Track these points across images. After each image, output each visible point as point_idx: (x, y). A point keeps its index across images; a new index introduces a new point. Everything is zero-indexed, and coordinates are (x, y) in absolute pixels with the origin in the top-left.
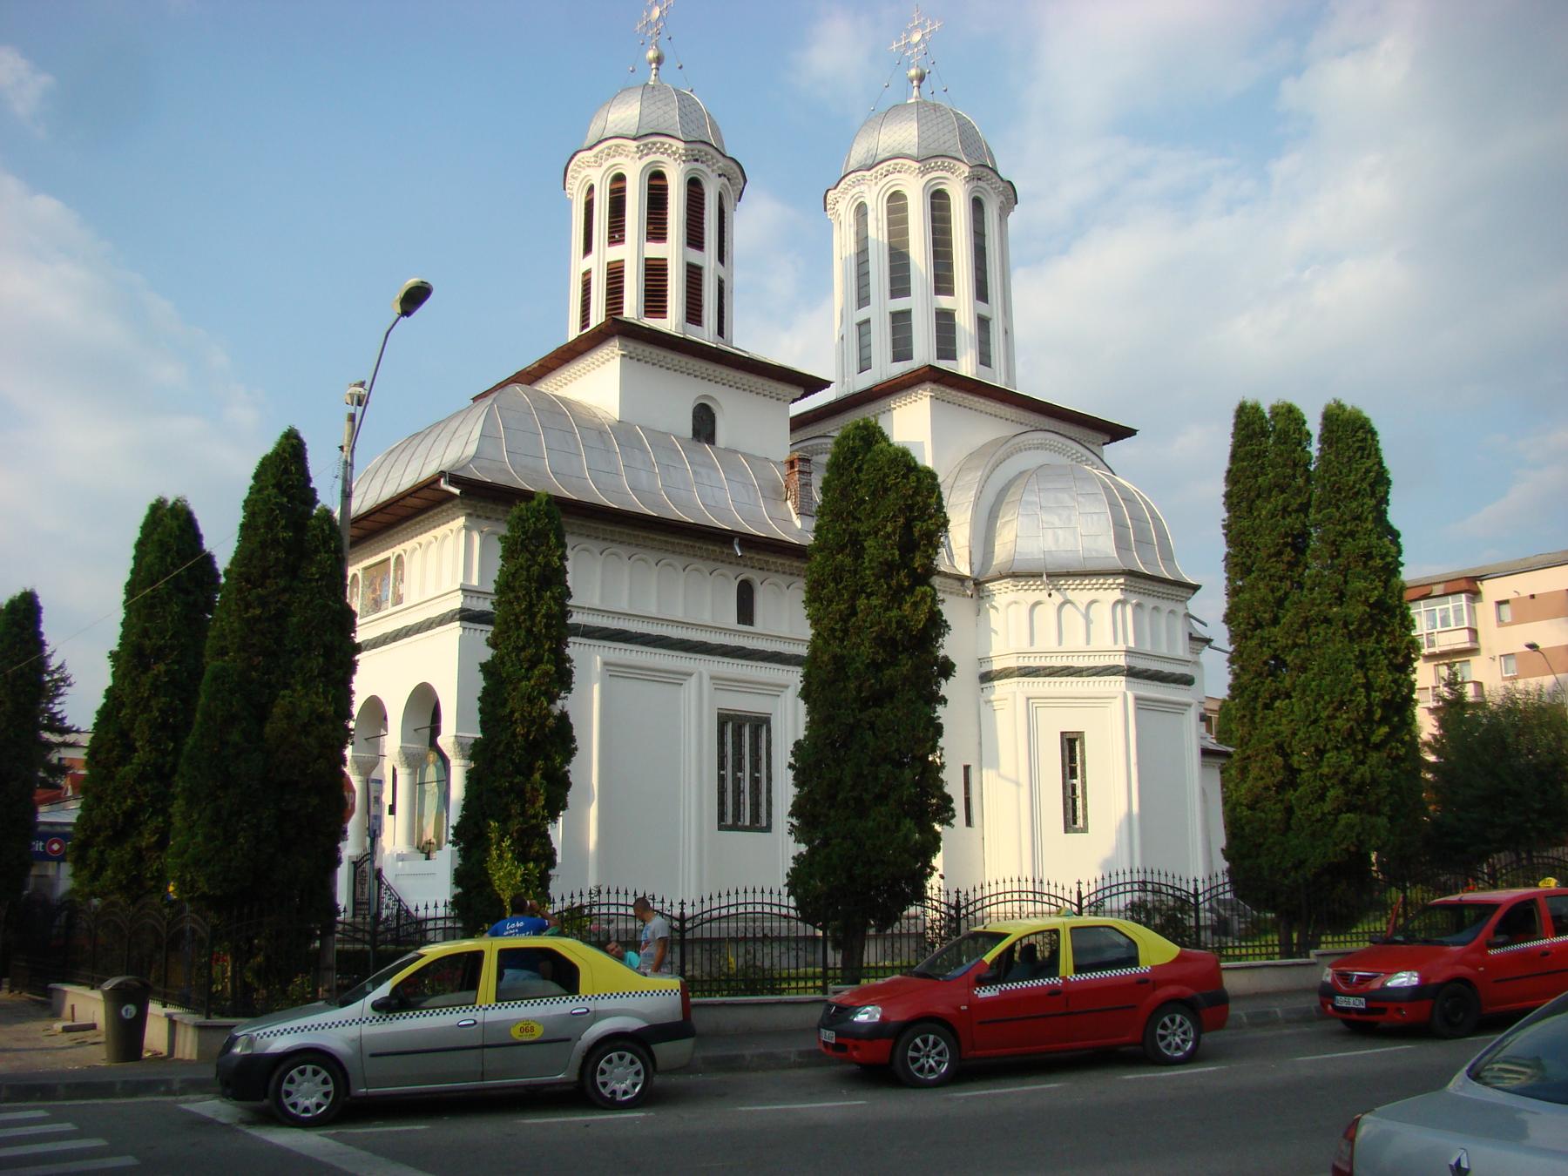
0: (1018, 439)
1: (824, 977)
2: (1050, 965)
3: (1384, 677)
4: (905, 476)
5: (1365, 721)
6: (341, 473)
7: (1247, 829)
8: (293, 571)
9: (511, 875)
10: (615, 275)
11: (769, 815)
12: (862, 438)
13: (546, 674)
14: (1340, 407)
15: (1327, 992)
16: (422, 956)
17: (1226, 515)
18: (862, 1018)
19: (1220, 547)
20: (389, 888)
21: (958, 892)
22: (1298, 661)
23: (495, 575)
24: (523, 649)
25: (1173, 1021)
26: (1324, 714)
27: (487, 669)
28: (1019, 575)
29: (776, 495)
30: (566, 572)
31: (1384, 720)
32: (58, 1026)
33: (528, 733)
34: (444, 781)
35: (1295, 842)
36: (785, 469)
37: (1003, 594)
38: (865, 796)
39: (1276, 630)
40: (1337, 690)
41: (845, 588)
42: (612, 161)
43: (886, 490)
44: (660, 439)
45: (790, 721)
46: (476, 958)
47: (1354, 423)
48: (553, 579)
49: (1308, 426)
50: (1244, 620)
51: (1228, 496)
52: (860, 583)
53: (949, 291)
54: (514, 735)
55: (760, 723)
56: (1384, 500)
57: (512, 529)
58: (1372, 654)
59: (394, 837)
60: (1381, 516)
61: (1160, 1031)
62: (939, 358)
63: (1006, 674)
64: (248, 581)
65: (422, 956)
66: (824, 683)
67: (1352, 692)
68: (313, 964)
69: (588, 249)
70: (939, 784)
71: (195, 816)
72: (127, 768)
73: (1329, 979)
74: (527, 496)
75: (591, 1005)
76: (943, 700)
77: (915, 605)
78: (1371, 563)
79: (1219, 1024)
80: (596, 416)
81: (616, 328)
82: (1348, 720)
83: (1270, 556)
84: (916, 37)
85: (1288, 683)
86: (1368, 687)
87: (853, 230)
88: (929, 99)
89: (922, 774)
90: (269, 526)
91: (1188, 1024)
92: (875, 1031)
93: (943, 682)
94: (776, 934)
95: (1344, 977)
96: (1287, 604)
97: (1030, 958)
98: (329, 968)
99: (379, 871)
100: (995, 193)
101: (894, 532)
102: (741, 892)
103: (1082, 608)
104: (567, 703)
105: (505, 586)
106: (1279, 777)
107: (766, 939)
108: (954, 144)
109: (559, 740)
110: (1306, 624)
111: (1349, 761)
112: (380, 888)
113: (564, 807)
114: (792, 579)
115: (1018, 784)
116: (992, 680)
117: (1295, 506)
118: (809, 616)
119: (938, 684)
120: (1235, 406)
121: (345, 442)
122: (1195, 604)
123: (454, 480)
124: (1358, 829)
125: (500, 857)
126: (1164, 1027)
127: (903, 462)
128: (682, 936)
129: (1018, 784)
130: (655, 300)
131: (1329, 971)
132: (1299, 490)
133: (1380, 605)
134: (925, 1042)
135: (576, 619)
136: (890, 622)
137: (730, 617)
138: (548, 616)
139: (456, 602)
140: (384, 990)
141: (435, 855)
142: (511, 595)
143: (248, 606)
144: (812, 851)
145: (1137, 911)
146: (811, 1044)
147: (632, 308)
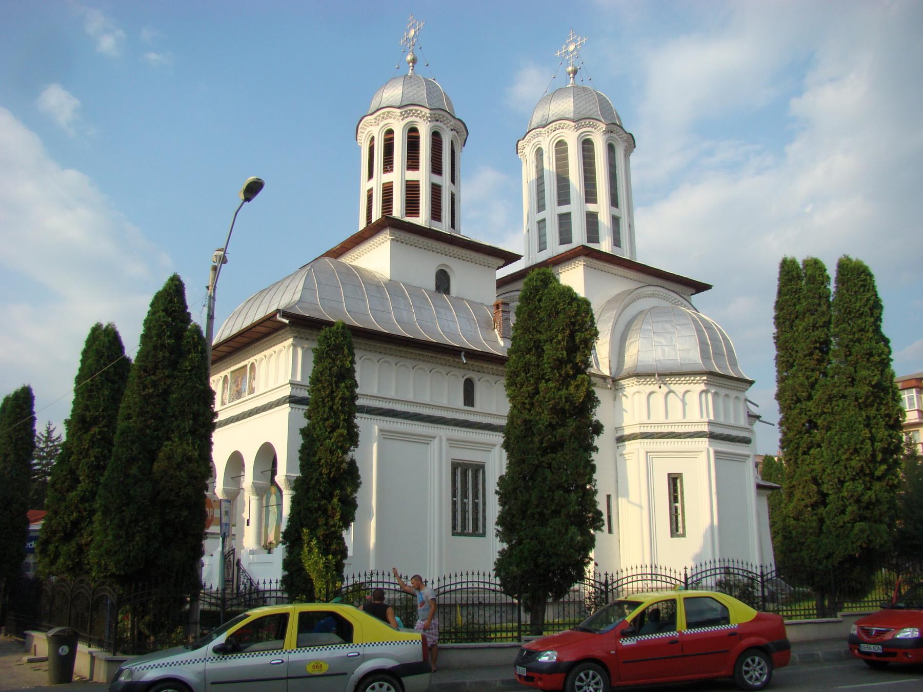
0: (636, 292)
1: (519, 629)
2: (670, 622)
3: (882, 433)
4: (570, 304)
5: (871, 461)
6: (207, 304)
7: (794, 532)
8: (174, 365)
9: (316, 563)
10: (388, 191)
11: (484, 526)
12: (541, 281)
13: (342, 435)
14: (849, 259)
15: (854, 642)
16: (248, 616)
17: (775, 331)
18: (544, 659)
19: (772, 351)
20: (244, 571)
21: (606, 574)
22: (825, 423)
23: (310, 373)
24: (327, 419)
25: (753, 661)
26: (843, 457)
27: (305, 432)
28: (640, 375)
29: (488, 326)
30: (354, 371)
31: (883, 461)
32: (25, 658)
33: (330, 473)
34: (280, 505)
35: (825, 541)
36: (494, 310)
37: (631, 387)
38: (546, 512)
39: (810, 403)
40: (852, 441)
41: (531, 376)
42: (385, 122)
43: (557, 313)
44: (415, 291)
45: (497, 464)
46: (283, 618)
47: (859, 269)
48: (346, 375)
49: (828, 273)
50: (789, 398)
51: (777, 318)
52: (541, 373)
53: (595, 201)
54: (321, 474)
55: (479, 468)
56: (879, 319)
57: (320, 345)
58: (874, 418)
59: (249, 539)
60: (877, 330)
61: (744, 668)
62: (588, 242)
63: (633, 437)
64: (145, 371)
65: (248, 616)
66: (518, 437)
67: (862, 443)
68: (185, 620)
69: (371, 175)
70: (594, 503)
71: (108, 523)
72: (74, 493)
73: (855, 632)
74: (330, 324)
75: (360, 650)
76: (596, 449)
77: (577, 387)
78: (871, 359)
79: (785, 663)
80: (375, 276)
81: (388, 222)
82: (860, 461)
83: (805, 356)
84: (572, 48)
85: (818, 437)
86: (873, 439)
87: (534, 165)
88: (581, 84)
89: (583, 497)
90: (159, 336)
91: (763, 663)
92: (553, 668)
93: (596, 437)
94: (487, 602)
95: (867, 632)
96: (817, 386)
97: (658, 617)
98: (196, 623)
99: (239, 561)
100: (622, 141)
101: (563, 340)
103: (681, 396)
104: (355, 454)
105: (316, 380)
106: (814, 499)
107: (481, 605)
108: (596, 111)
109: (349, 476)
110: (830, 399)
111: (860, 488)
112: (238, 571)
113: (353, 520)
114: (498, 378)
115: (641, 507)
116: (624, 441)
117: (821, 323)
118: (508, 395)
119: (592, 438)
120: (780, 260)
121: (210, 283)
122: (751, 393)
123: (285, 314)
124: (868, 532)
125: (310, 551)
126: (748, 665)
127: (568, 294)
129: (641, 507)
130: (412, 206)
131: (855, 627)
132: (823, 313)
133: (878, 385)
134: (587, 675)
136: (561, 398)
137: (459, 402)
138: (342, 398)
139: (287, 391)
140: (221, 639)
141: (275, 550)
142: (320, 386)
143: (145, 387)
144: (511, 548)
145: (723, 586)
146: (510, 675)
147: (398, 210)
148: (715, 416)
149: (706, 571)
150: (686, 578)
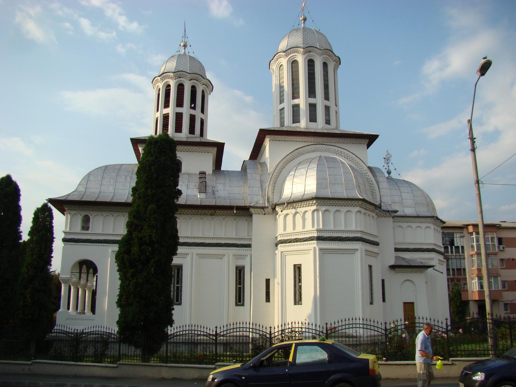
103: (302, 214)
135: (181, 240)
148: (323, 226)
149: (186, 330)
150: (327, 330)
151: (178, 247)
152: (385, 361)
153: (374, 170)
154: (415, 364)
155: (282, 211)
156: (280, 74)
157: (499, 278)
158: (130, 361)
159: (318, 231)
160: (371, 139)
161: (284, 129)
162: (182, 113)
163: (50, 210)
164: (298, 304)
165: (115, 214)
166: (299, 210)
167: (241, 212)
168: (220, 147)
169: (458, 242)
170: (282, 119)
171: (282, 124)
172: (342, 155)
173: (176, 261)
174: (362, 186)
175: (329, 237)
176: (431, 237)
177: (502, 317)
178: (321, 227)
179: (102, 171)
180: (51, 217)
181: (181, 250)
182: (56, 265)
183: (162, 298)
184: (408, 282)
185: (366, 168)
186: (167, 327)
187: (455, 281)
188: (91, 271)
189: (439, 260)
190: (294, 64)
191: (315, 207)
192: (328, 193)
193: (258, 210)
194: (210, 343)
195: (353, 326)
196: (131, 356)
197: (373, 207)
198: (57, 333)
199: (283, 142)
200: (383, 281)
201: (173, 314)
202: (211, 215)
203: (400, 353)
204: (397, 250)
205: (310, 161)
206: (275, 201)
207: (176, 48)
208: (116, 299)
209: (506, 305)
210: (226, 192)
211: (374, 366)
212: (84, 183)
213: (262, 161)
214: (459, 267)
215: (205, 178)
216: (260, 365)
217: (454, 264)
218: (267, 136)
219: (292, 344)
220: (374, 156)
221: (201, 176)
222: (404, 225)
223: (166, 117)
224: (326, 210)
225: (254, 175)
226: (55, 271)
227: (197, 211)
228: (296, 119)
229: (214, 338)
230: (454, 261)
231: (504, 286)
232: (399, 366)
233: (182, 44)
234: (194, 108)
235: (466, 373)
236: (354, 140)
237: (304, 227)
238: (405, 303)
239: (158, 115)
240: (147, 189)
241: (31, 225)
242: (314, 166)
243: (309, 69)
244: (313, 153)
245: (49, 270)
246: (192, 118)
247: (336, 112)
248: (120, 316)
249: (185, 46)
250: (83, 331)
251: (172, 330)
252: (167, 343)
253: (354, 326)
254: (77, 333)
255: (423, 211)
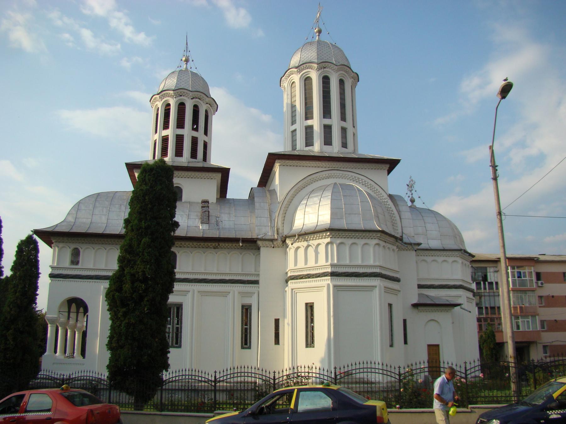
37: (292, 246)
102: (246, 367)
103: (314, 247)
128: (274, 382)
135: (178, 276)
151: (175, 283)
152: (399, 408)
153: (396, 198)
154: (433, 412)
155: (292, 244)
156: (291, 91)
157: (537, 317)
158: (127, 409)
159: (332, 265)
160: (392, 164)
161: (296, 153)
162: (183, 136)
163: (36, 243)
164: (310, 347)
165: (97, 247)
166: (311, 242)
167: (248, 245)
168: (225, 173)
169: (491, 277)
170: (294, 141)
171: (294, 147)
172: (359, 182)
173: (173, 299)
174: (381, 216)
175: (345, 273)
176: (459, 272)
177: (536, 361)
178: (336, 262)
179: (94, 199)
180: (36, 250)
181: (177, 287)
182: (42, 303)
183: (157, 340)
184: (433, 323)
185: (386, 196)
186: (162, 372)
187: (489, 321)
188: (81, 310)
189: (467, 298)
190: (307, 81)
191: (328, 240)
192: (337, 225)
193: (267, 243)
194: (208, 390)
195: (371, 370)
196: (125, 403)
197: (394, 239)
198: (43, 378)
199: (295, 167)
200: (405, 321)
201: (168, 358)
202: (214, 248)
203: (415, 400)
204: (420, 286)
205: (323, 189)
206: (286, 233)
207: (177, 64)
208: (106, 341)
209: (545, 347)
210: (231, 223)
211: (382, 414)
212: (74, 212)
213: (271, 188)
214: (492, 305)
215: (208, 207)
216: (260, 412)
217: (486, 303)
218: (276, 161)
219: (294, 390)
220: (395, 182)
221: (204, 205)
222: (429, 259)
223: (165, 140)
224: (341, 243)
225: (262, 204)
226: (41, 311)
227: (199, 244)
228: (309, 142)
229: (213, 384)
230: (487, 298)
231: (543, 326)
232: (413, 414)
233: (184, 59)
234: (196, 130)
235: (481, 422)
236: (374, 165)
237: (316, 261)
238: (429, 346)
239: (157, 137)
240: (140, 220)
241: (15, 259)
242: (328, 194)
243: (324, 87)
244: (328, 180)
245: (35, 308)
246: (194, 141)
247: (354, 135)
248: (111, 360)
249: (187, 61)
250: (70, 377)
251: (168, 375)
252: (162, 390)
253: (373, 370)
254: (63, 379)
255: (450, 244)
